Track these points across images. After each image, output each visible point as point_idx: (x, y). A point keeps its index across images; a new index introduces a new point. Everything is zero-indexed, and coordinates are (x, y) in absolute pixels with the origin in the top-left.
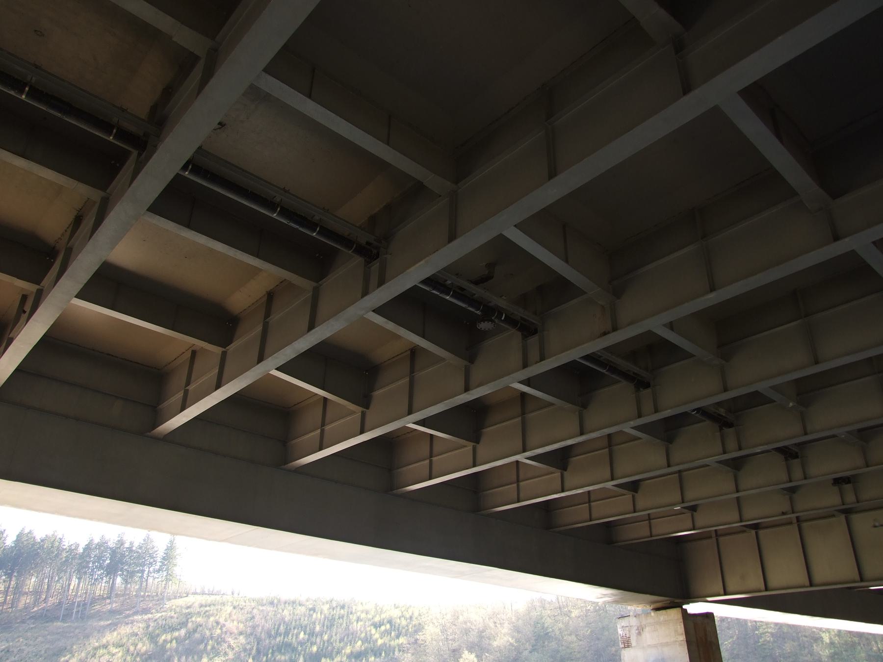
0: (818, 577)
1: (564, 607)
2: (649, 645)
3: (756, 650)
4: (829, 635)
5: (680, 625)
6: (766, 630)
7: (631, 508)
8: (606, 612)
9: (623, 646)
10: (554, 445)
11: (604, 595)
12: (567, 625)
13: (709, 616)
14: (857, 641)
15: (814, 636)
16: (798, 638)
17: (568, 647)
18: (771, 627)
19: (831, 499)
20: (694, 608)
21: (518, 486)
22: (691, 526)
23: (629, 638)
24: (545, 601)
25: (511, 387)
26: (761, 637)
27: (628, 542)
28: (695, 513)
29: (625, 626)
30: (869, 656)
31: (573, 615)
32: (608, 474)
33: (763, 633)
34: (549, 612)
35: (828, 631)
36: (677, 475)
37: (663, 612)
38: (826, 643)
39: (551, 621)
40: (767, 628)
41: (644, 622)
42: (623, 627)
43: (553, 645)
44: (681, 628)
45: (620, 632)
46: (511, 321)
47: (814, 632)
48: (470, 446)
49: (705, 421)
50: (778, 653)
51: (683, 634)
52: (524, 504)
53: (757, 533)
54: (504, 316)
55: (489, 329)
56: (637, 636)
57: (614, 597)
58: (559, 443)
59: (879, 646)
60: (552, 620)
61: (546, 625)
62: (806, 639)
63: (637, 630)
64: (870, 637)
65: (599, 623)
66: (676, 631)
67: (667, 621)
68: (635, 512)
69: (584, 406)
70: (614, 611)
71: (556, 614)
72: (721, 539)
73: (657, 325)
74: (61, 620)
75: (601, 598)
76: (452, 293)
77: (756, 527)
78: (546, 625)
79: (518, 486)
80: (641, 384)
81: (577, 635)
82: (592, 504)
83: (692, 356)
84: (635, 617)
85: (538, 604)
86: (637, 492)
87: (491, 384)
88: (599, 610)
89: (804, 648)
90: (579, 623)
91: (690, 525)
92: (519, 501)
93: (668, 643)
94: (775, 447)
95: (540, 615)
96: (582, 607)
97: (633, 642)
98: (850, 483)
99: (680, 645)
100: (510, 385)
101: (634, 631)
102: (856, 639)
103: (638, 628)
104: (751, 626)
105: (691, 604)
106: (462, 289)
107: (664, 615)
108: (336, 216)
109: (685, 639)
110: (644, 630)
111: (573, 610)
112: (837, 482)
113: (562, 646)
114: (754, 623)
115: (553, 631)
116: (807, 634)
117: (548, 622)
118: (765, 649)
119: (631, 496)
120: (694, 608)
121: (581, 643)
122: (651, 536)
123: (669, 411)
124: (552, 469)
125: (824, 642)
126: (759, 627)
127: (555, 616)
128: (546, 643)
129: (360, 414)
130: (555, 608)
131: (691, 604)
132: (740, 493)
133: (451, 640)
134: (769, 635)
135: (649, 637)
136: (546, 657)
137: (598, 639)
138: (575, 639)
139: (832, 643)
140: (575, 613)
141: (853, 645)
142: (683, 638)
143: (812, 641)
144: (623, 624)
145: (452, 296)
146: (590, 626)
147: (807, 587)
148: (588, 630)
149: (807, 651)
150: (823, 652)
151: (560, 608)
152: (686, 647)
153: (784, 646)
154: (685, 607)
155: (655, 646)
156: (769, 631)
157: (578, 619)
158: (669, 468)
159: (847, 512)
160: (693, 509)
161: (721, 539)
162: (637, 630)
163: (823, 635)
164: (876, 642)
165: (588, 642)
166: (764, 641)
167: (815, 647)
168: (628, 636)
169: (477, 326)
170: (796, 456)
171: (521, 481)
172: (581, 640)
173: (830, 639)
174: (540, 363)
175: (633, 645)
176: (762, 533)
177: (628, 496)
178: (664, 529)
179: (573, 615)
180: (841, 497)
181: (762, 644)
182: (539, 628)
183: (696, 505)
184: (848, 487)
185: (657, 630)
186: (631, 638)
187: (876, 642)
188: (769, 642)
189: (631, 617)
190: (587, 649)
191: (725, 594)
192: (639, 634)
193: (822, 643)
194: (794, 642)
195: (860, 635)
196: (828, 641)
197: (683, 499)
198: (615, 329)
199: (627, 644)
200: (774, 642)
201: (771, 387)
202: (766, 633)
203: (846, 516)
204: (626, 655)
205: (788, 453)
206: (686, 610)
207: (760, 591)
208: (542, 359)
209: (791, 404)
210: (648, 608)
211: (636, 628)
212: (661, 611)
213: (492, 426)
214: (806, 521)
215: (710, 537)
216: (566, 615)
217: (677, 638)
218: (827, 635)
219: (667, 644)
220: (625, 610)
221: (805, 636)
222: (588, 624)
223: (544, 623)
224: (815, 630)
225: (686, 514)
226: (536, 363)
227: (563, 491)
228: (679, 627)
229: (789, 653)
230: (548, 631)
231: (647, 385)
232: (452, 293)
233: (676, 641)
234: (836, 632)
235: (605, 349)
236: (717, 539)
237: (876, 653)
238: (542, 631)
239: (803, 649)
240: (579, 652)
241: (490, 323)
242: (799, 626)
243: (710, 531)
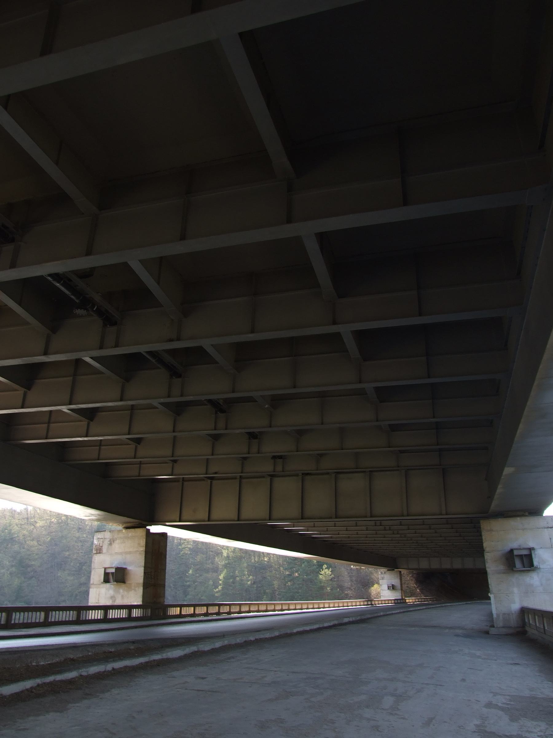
0: (244, 515)
1: (31, 518)
2: (117, 553)
3: (176, 559)
4: (228, 551)
5: (143, 540)
6: (187, 546)
8: (68, 524)
9: (95, 552)
10: (97, 404)
11: (92, 514)
12: (31, 532)
13: (164, 535)
14: (244, 556)
15: (217, 551)
16: (207, 553)
17: (28, 550)
18: (190, 544)
19: (268, 468)
20: (155, 529)
21: (48, 427)
23: (102, 546)
24: (15, 511)
25: (82, 359)
26: (182, 551)
27: (120, 478)
28: (175, 464)
29: (100, 538)
30: (249, 565)
31: (38, 525)
32: (126, 429)
33: (184, 548)
34: (17, 521)
35: (228, 548)
36: (128, 412)
37: (133, 530)
38: (224, 557)
39: (17, 528)
40: (188, 545)
41: (116, 536)
42: (98, 538)
43: (16, 547)
44: (143, 542)
45: (96, 542)
46: (100, 313)
47: (219, 549)
48: (21, 391)
49: (206, 405)
50: (191, 562)
51: (143, 546)
52: (51, 441)
53: (211, 483)
54: (96, 308)
55: (79, 314)
56: (108, 546)
57: (99, 517)
58: (102, 403)
59: (256, 559)
60: (19, 527)
61: (13, 531)
62: (211, 553)
63: (109, 541)
64: (287, 557)
65: (60, 533)
66: (139, 544)
67: (134, 536)
68: (135, 458)
69: (54, 330)
70: (74, 525)
71: (23, 523)
72: (185, 483)
73: (206, 344)
74: (469, 564)
75: (89, 516)
76: (62, 282)
77: (212, 479)
78: (13, 531)
79: (48, 427)
80: (174, 373)
81: (38, 541)
82: (102, 447)
83: (217, 363)
84: (110, 532)
85: (8, 514)
86: (29, 389)
87: (69, 355)
88: (61, 523)
89: (209, 559)
90: (42, 532)
91: (170, 471)
92: (46, 438)
93: (131, 552)
94: (247, 431)
95: (9, 523)
96: (47, 519)
97: (104, 550)
98: (282, 459)
99: (140, 554)
100: (82, 358)
101: (107, 542)
102: (243, 555)
103: (110, 540)
104: (177, 542)
105: (153, 526)
106: (70, 280)
107: (132, 533)
109: (144, 550)
110: (115, 541)
111: (38, 521)
112: (274, 457)
113: (24, 548)
114: (179, 541)
115: (18, 537)
116: (213, 550)
117: (16, 529)
118: (183, 558)
119: (135, 446)
120: (155, 529)
121: (40, 547)
122: (139, 476)
123: (192, 397)
124: (83, 419)
125: (223, 556)
126: (182, 543)
127: (21, 525)
128: (9, 546)
129: (23, 392)
130: (24, 519)
131: (153, 526)
132: (214, 456)
134: (188, 549)
135: (117, 547)
136: (7, 557)
137: (56, 545)
138: (36, 544)
139: (228, 557)
140: (40, 524)
141: (241, 558)
142: (143, 549)
143: (215, 555)
144: (99, 537)
145: (62, 285)
146: (51, 534)
147: (236, 521)
148: (49, 538)
149: (210, 561)
150: (221, 563)
151: (27, 519)
152: (144, 556)
153: (196, 557)
154: (148, 527)
155: (121, 554)
156: (189, 547)
157: (41, 528)
158: (174, 433)
159: (272, 476)
160: (175, 461)
161: (185, 483)
162: (109, 541)
163: (223, 551)
164: (255, 557)
165: (47, 547)
166: (183, 553)
167: (216, 559)
168: (101, 545)
169: (74, 311)
171: (52, 423)
172: (40, 545)
173: (228, 554)
174: (114, 348)
175: (103, 552)
176: (214, 482)
177: (133, 446)
178: (148, 472)
179: (38, 525)
181: (182, 556)
182: (5, 533)
183: (143, 438)
184: (279, 461)
185: (125, 542)
186: (103, 547)
187: (255, 557)
188: (187, 554)
189: (106, 532)
190: (45, 552)
191: (180, 521)
192: (110, 544)
193: (222, 556)
194: (204, 555)
195: (246, 552)
196: (226, 555)
197: (173, 454)
198: (178, 339)
199: (99, 551)
200: (191, 554)
201: (261, 396)
202: (186, 548)
203: (271, 478)
204: (96, 559)
205: (252, 436)
206: (149, 530)
207: (204, 521)
208: (117, 346)
209: (267, 406)
210: (120, 527)
211: (109, 540)
212: (131, 530)
213: (45, 379)
215: (179, 481)
216: (31, 524)
217: (139, 549)
218: (226, 551)
219: (130, 553)
220: (83, 525)
221: (212, 552)
222: (49, 533)
223: (11, 530)
224: (219, 548)
225: (168, 464)
226: (111, 348)
227: (87, 436)
228: (142, 541)
229: (198, 562)
230: (14, 536)
231: (179, 376)
232: (62, 282)
233: (137, 551)
234: (232, 550)
235: (164, 350)
236: (183, 483)
237: (253, 563)
238: (9, 535)
239: (208, 560)
240: (37, 554)
241: (86, 311)
242: (210, 543)
243: (179, 478)
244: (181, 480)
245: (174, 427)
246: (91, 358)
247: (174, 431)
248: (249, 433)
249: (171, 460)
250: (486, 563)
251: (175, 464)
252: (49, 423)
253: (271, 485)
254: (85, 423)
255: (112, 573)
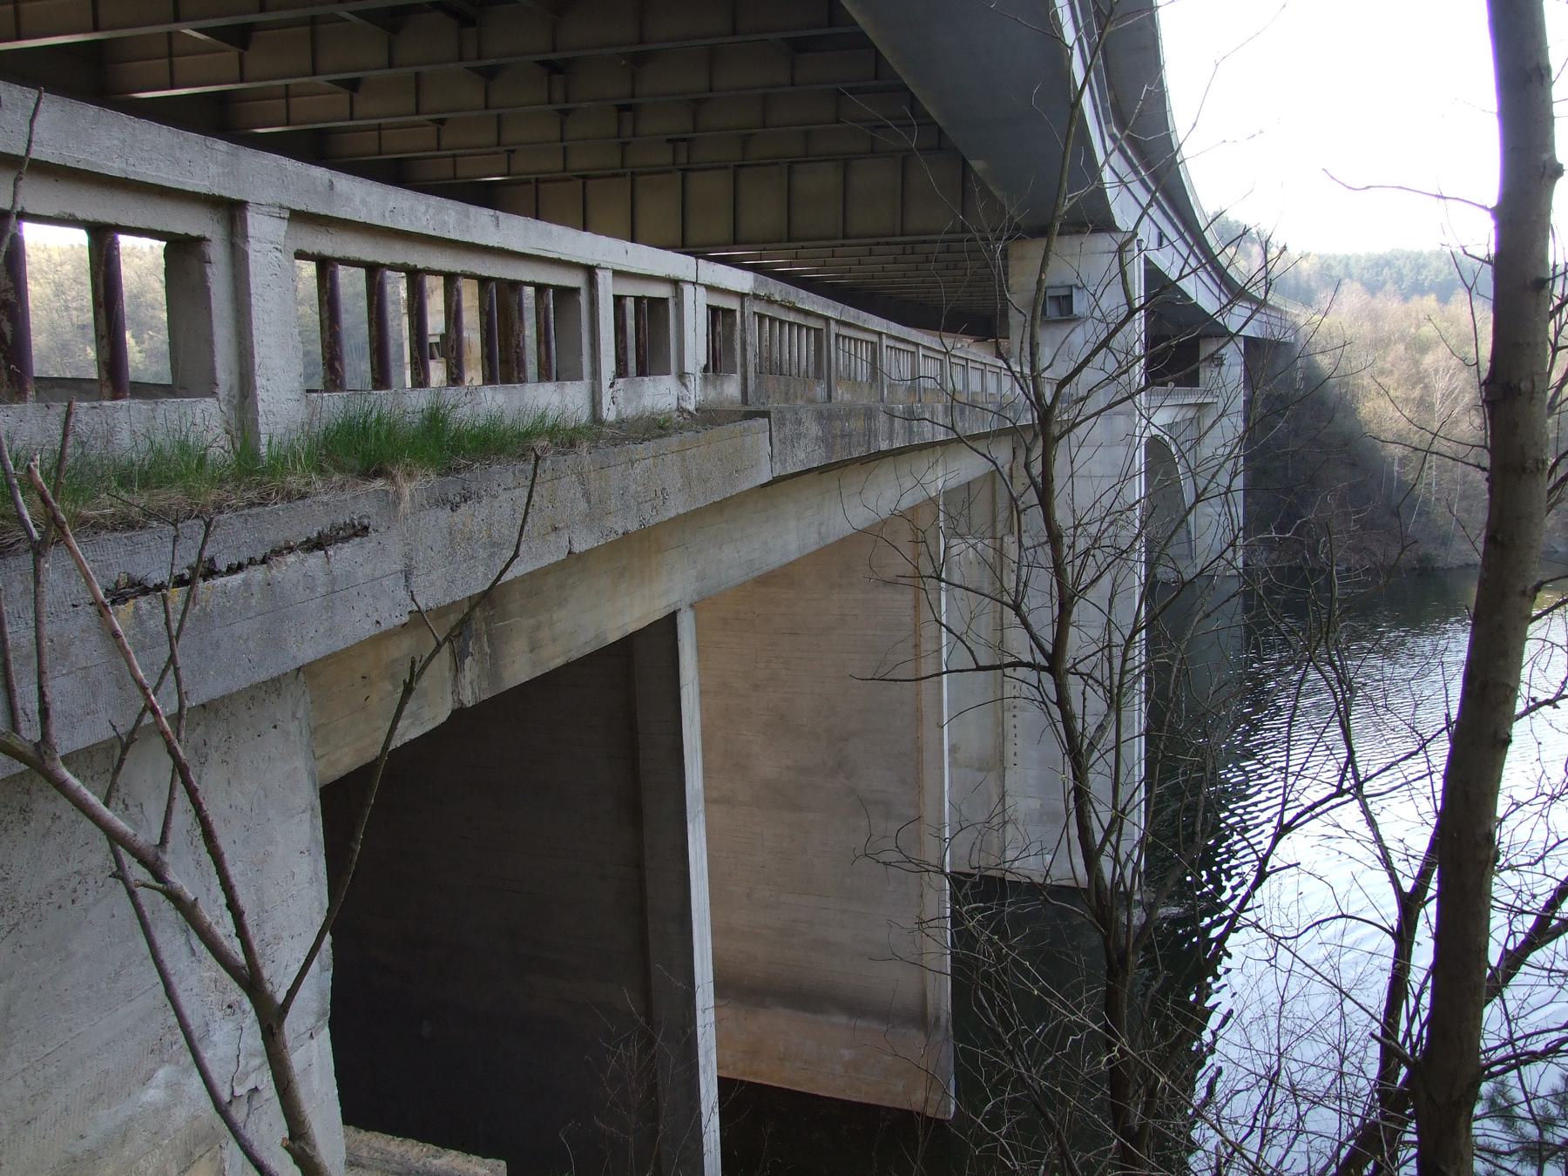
7: (434, 144)
22: (505, 171)
36: (307, 29)
53: (584, 183)
68: (352, 119)
72: (542, 186)
74: (532, 368)
108: (832, 160)
124: (225, 46)
133: (75, 309)
170: (560, 72)
176: (590, 183)
177: (344, 96)
180: (734, 185)
183: (445, 119)
184: (628, 115)
214: (642, 174)
236: (537, 186)
244: (533, 181)
245: (562, 135)
246: (351, 12)
247: (562, 140)
248: (542, 63)
249: (430, 120)
250: (465, 369)
251: (512, 155)
252: (171, 55)
253: (683, 186)
254: (233, 53)
255: (437, 344)
